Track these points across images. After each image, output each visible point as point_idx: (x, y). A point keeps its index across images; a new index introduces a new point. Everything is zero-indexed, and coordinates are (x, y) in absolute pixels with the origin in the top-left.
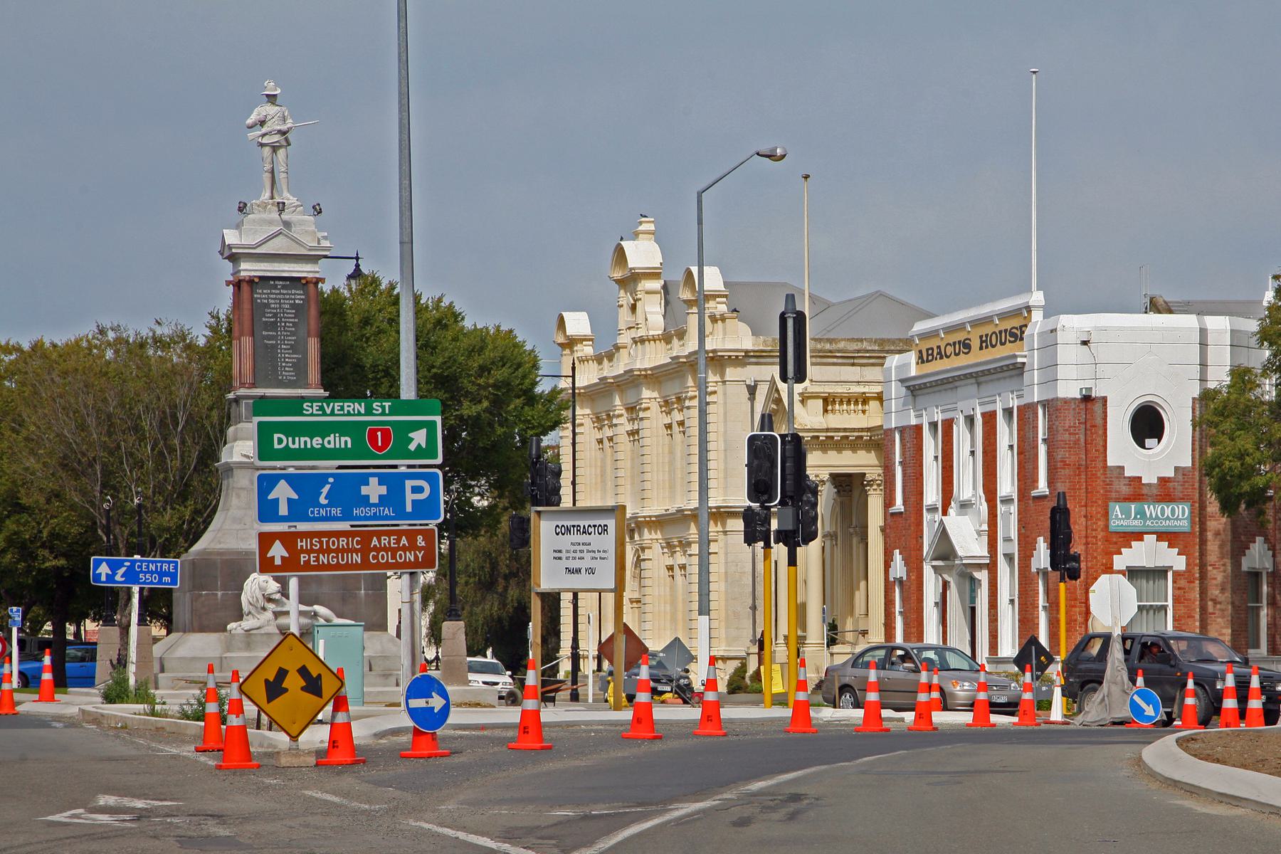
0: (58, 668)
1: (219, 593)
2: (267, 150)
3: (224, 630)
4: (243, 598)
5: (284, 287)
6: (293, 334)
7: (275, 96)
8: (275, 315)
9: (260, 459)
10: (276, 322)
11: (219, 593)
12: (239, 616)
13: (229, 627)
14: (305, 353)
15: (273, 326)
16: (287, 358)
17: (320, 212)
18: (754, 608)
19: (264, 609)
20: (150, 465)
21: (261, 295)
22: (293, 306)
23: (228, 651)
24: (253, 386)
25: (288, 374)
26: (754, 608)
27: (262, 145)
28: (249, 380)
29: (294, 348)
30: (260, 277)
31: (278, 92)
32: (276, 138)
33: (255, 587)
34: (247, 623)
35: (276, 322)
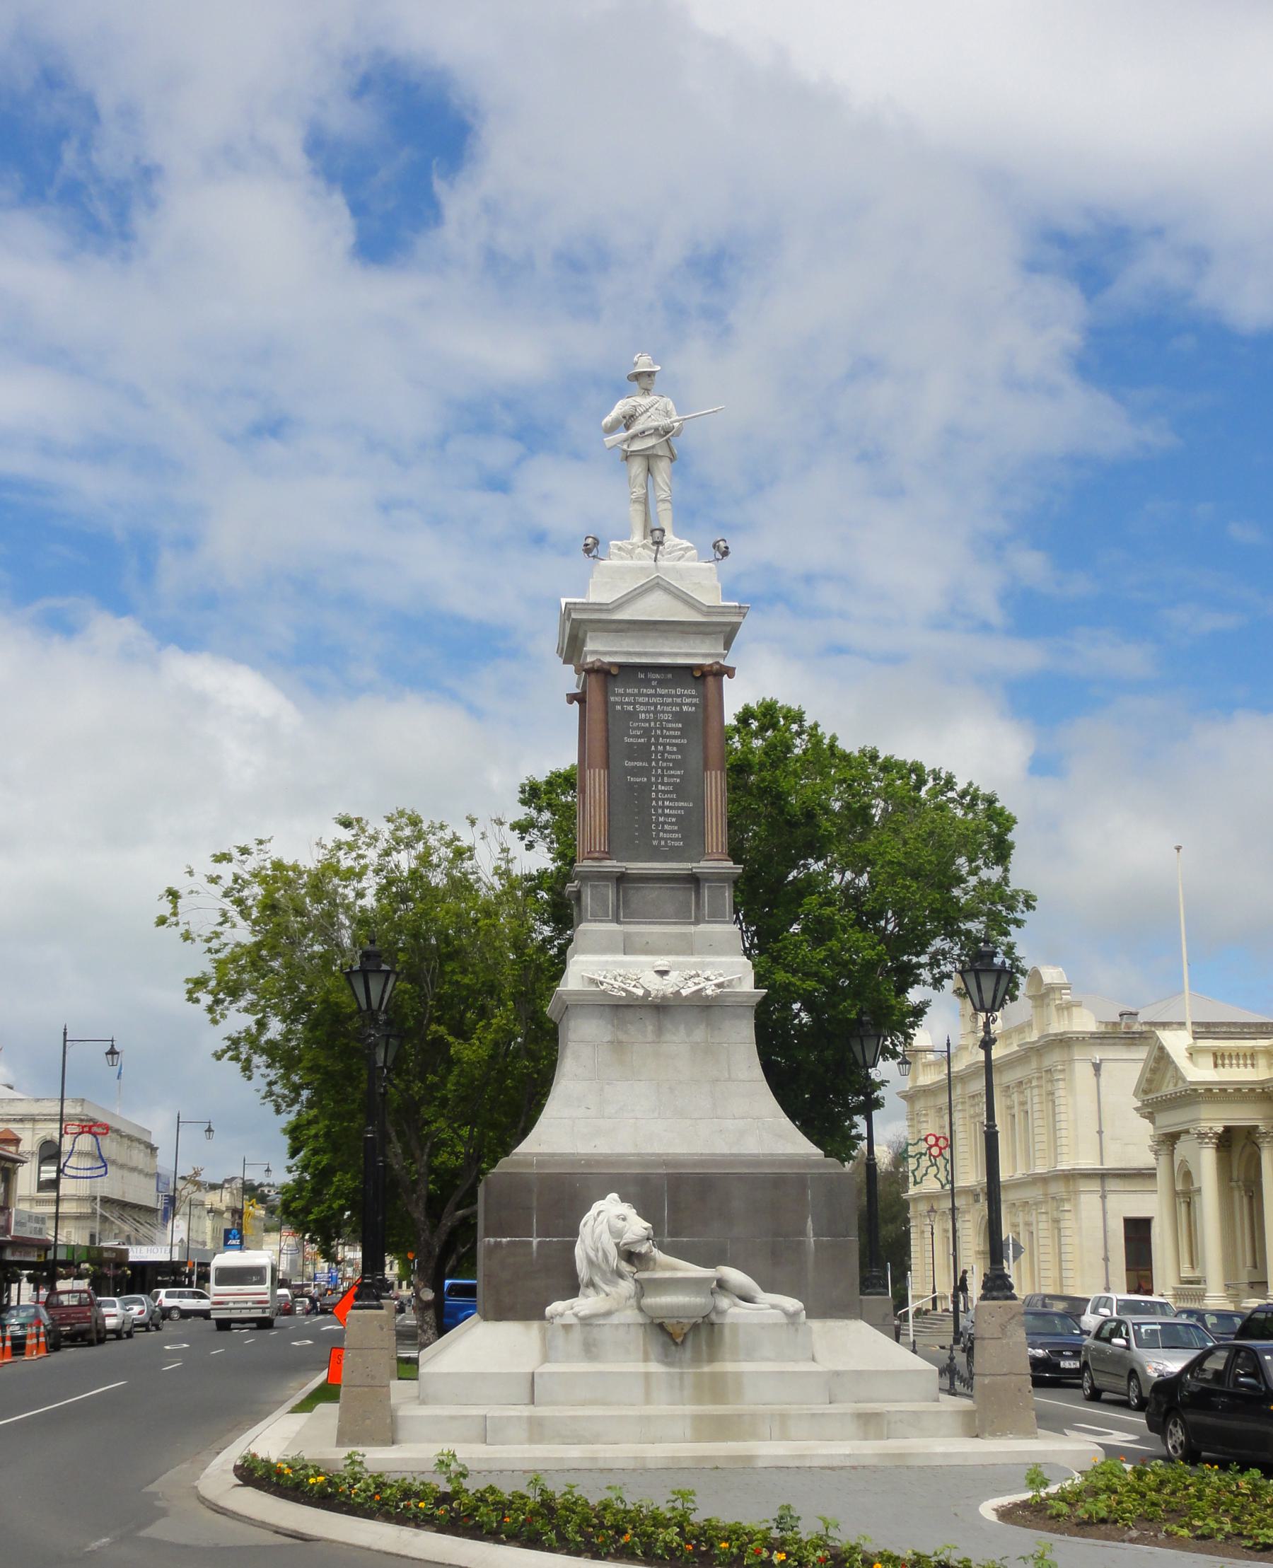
0: (522, 994)
1: (535, 1241)
2: (637, 467)
3: (542, 1317)
4: (579, 1251)
5: (661, 683)
6: (677, 765)
7: (653, 373)
8: (647, 732)
9: (217, 1269)
10: (649, 744)
11: (535, 1241)
12: (572, 1288)
13: (549, 1310)
14: (700, 800)
15: (642, 752)
16: (669, 808)
17: (725, 553)
18: (1106, 1259)
19: (620, 1275)
20: (420, 847)
21: (623, 696)
22: (678, 716)
23: (546, 1359)
24: (608, 855)
25: (670, 836)
26: (1106, 1259)
27: (628, 456)
28: (600, 845)
29: (679, 791)
30: (622, 666)
31: (657, 368)
32: (650, 442)
33: (602, 1228)
34: (585, 1304)
35: (649, 744)
